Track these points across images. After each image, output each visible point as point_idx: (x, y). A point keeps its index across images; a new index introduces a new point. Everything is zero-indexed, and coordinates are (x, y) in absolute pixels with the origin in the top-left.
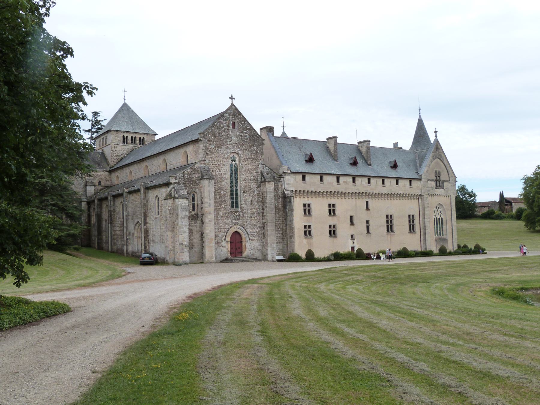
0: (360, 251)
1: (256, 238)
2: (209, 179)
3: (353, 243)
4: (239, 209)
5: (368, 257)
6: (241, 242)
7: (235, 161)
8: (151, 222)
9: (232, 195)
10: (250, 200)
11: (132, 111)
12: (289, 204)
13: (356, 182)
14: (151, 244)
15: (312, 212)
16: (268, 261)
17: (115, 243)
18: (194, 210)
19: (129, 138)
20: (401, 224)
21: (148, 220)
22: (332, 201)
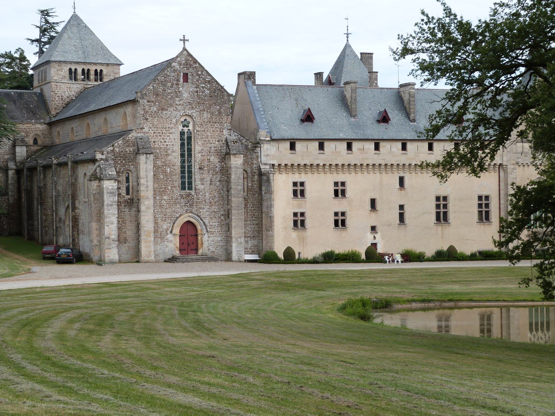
0: (452, 249)
1: (216, 230)
2: (147, 154)
3: (375, 237)
4: (193, 192)
5: (462, 258)
6: (196, 235)
7: (188, 127)
8: (80, 207)
9: (183, 172)
10: (208, 179)
11: (86, 27)
12: (266, 184)
13: (381, 149)
14: (81, 236)
15: (307, 194)
16: (232, 261)
17: (46, 232)
18: (128, 193)
19: (80, 71)
20: (463, 212)
21: (77, 205)
22: (340, 178)
